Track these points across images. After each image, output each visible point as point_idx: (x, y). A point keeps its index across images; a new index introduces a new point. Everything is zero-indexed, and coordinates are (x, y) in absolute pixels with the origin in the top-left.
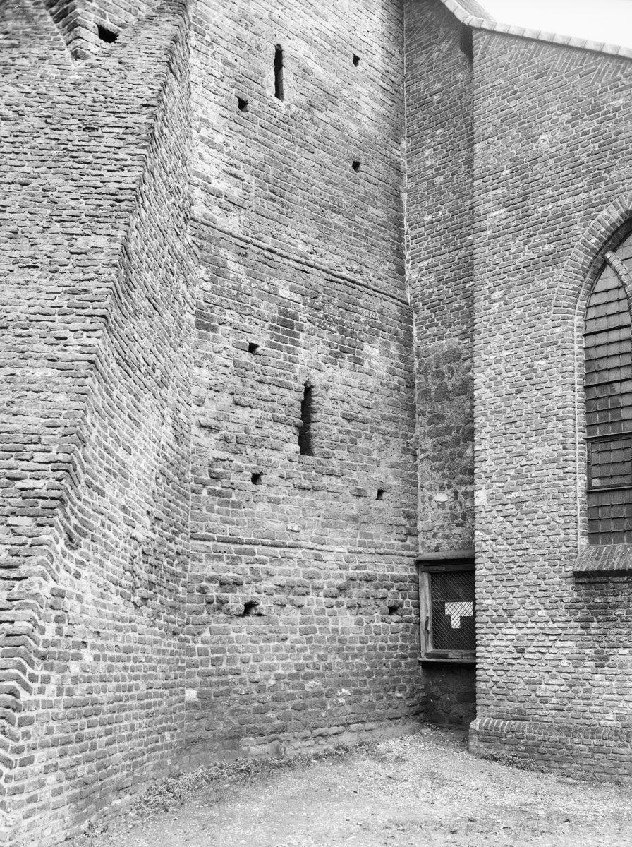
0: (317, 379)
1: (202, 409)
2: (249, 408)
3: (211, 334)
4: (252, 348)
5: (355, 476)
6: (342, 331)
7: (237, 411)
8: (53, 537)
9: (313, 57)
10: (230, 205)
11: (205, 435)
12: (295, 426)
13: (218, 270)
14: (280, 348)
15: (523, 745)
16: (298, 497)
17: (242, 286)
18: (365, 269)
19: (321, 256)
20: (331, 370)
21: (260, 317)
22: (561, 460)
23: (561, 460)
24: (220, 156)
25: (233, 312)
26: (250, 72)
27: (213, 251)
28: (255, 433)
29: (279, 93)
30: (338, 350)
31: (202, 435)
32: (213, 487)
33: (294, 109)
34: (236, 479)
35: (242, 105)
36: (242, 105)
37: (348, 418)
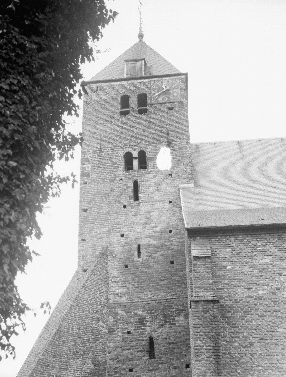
0: (154, 335)
1: (111, 354)
2: (127, 350)
3: (113, 333)
4: (129, 333)
5: (173, 362)
6: (165, 317)
7: (123, 352)
8: (60, 178)
9: (152, 240)
10: (121, 295)
11: (112, 361)
12: (146, 351)
13: (115, 314)
14: (138, 329)
15: (64, 353)
16: (149, 373)
17: (124, 316)
18: (177, 293)
19: (158, 296)
20: (161, 330)
21: (131, 322)
22: (241, 337)
23: (241, 337)
24: (119, 283)
25: (121, 324)
26: (128, 257)
27: (114, 311)
28: (130, 357)
29: (139, 256)
30: (163, 323)
31: (111, 362)
32: (115, 376)
33: (145, 258)
34: (123, 372)
35: (126, 267)
36: (126, 267)
37: (169, 344)
